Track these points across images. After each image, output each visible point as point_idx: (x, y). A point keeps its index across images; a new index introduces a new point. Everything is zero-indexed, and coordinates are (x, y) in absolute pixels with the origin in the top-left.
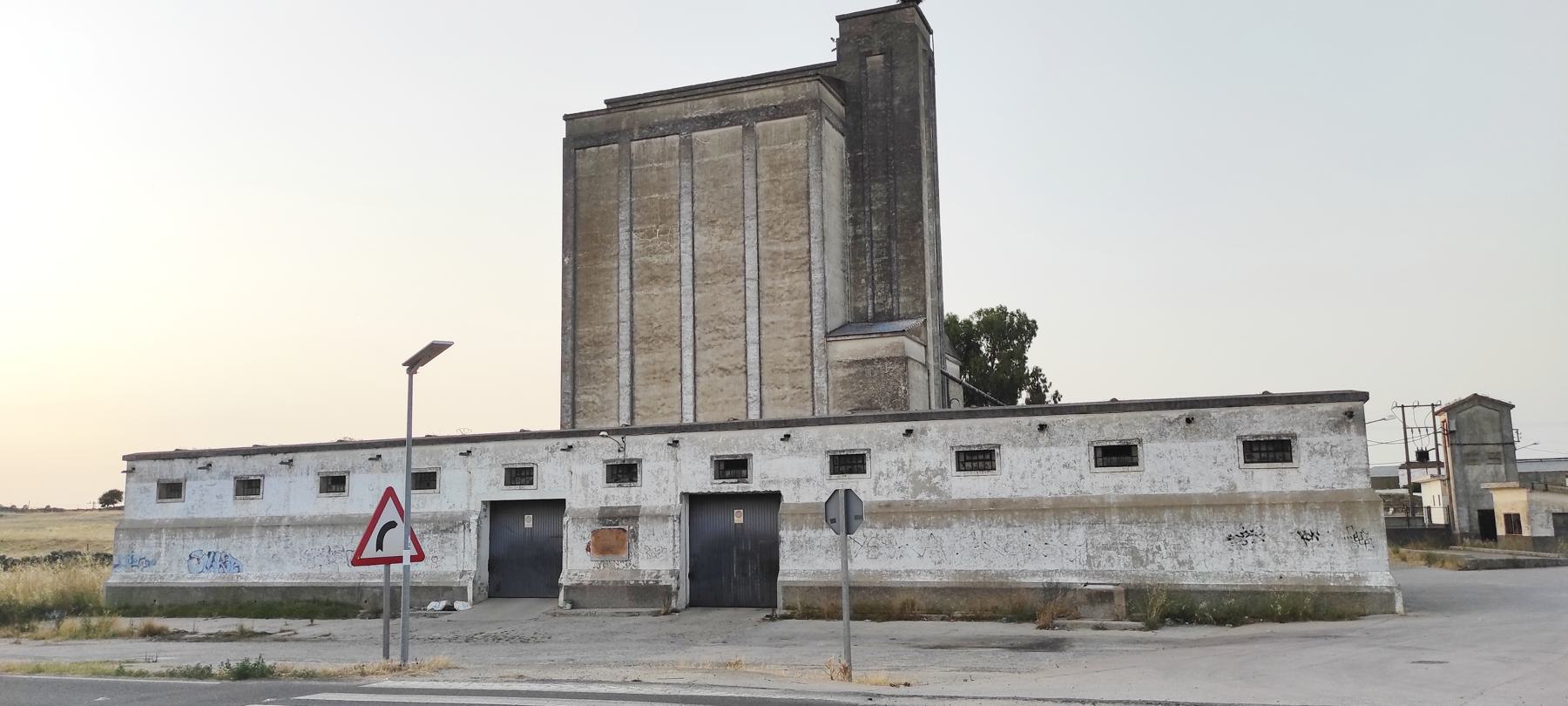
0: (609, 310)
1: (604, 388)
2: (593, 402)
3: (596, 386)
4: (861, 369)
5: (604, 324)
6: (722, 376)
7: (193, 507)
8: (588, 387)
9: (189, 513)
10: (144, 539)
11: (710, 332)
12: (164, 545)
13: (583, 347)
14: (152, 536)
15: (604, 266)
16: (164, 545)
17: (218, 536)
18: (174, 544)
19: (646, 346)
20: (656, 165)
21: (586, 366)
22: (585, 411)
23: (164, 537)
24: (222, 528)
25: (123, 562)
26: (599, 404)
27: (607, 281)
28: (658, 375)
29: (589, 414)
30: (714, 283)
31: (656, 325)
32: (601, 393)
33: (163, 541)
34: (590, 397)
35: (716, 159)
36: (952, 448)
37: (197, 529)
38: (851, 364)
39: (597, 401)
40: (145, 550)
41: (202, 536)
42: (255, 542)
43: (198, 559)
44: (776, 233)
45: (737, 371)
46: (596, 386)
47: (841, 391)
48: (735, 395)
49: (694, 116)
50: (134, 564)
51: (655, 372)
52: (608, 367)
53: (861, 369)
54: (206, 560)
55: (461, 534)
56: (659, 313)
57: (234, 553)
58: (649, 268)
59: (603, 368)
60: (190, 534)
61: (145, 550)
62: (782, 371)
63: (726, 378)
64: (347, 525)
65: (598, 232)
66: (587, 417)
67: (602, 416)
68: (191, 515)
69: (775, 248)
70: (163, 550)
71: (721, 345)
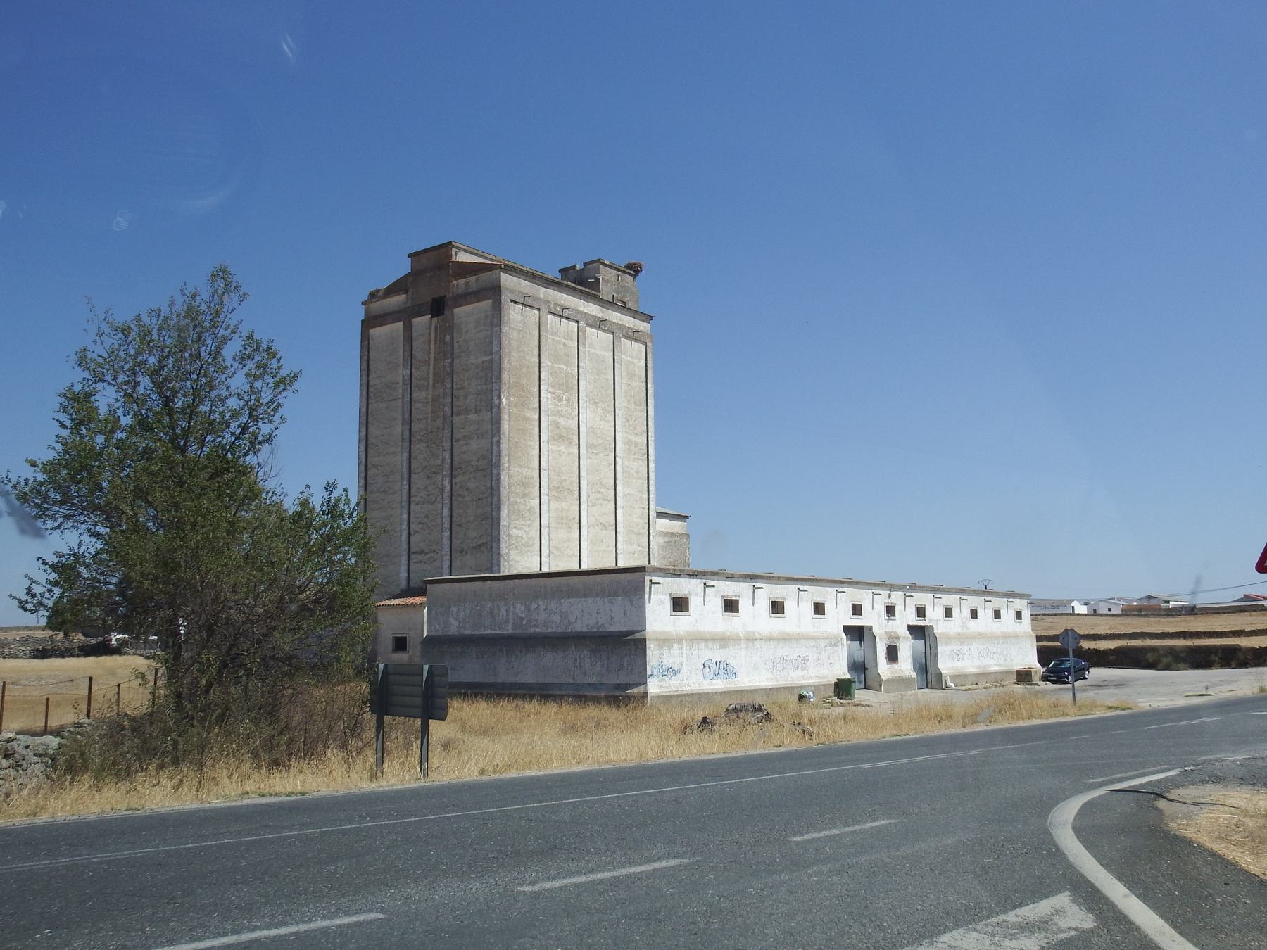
0: (532, 456)
1: (529, 525)
2: (522, 537)
3: (523, 523)
4: (670, 539)
5: (528, 468)
6: (602, 530)
7: (696, 620)
8: (518, 522)
9: (694, 626)
10: (670, 649)
11: (595, 492)
12: (685, 655)
13: (514, 485)
14: (675, 646)
15: (528, 415)
16: (685, 655)
17: (721, 647)
18: (692, 654)
19: (557, 495)
20: (563, 340)
21: (516, 502)
22: (516, 544)
23: (685, 647)
24: (722, 640)
25: (655, 673)
26: (526, 540)
27: (531, 429)
28: (564, 521)
29: (519, 548)
30: (597, 454)
31: (563, 478)
32: (527, 530)
33: (684, 651)
34: (520, 531)
35: (598, 352)
36: (770, 599)
37: (706, 640)
38: (667, 534)
39: (524, 536)
40: (671, 660)
41: (710, 646)
42: (743, 652)
43: (709, 668)
44: (630, 426)
45: (610, 527)
46: (523, 523)
47: (662, 552)
48: (608, 546)
49: (585, 311)
50: (664, 673)
51: (562, 519)
52: (532, 507)
53: (670, 539)
54: (714, 668)
55: (840, 647)
56: (565, 468)
57: (732, 662)
58: (558, 428)
59: (528, 508)
60: (702, 645)
61: (671, 660)
62: (633, 532)
63: (604, 532)
64: (791, 639)
65: (524, 382)
66: (518, 550)
67: (528, 551)
68: (695, 628)
69: (630, 437)
70: (685, 660)
71: (601, 504)
